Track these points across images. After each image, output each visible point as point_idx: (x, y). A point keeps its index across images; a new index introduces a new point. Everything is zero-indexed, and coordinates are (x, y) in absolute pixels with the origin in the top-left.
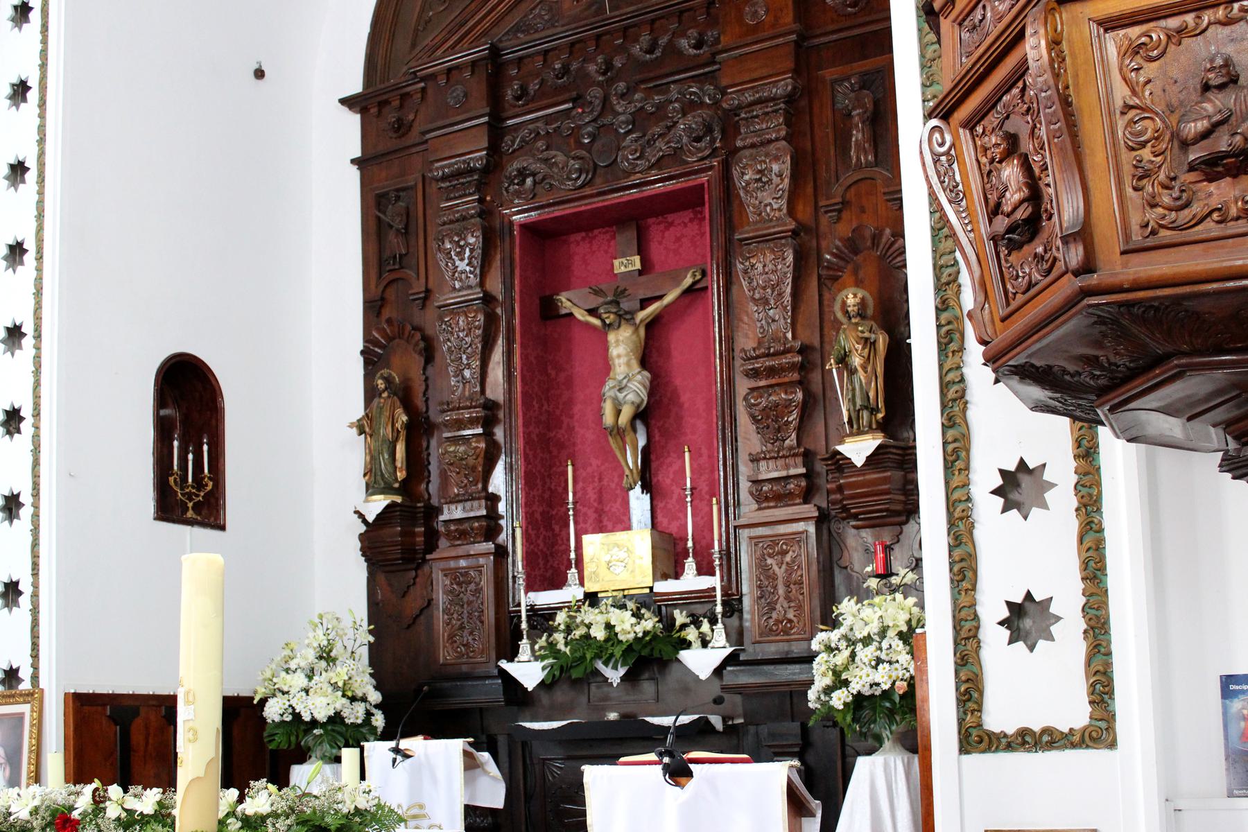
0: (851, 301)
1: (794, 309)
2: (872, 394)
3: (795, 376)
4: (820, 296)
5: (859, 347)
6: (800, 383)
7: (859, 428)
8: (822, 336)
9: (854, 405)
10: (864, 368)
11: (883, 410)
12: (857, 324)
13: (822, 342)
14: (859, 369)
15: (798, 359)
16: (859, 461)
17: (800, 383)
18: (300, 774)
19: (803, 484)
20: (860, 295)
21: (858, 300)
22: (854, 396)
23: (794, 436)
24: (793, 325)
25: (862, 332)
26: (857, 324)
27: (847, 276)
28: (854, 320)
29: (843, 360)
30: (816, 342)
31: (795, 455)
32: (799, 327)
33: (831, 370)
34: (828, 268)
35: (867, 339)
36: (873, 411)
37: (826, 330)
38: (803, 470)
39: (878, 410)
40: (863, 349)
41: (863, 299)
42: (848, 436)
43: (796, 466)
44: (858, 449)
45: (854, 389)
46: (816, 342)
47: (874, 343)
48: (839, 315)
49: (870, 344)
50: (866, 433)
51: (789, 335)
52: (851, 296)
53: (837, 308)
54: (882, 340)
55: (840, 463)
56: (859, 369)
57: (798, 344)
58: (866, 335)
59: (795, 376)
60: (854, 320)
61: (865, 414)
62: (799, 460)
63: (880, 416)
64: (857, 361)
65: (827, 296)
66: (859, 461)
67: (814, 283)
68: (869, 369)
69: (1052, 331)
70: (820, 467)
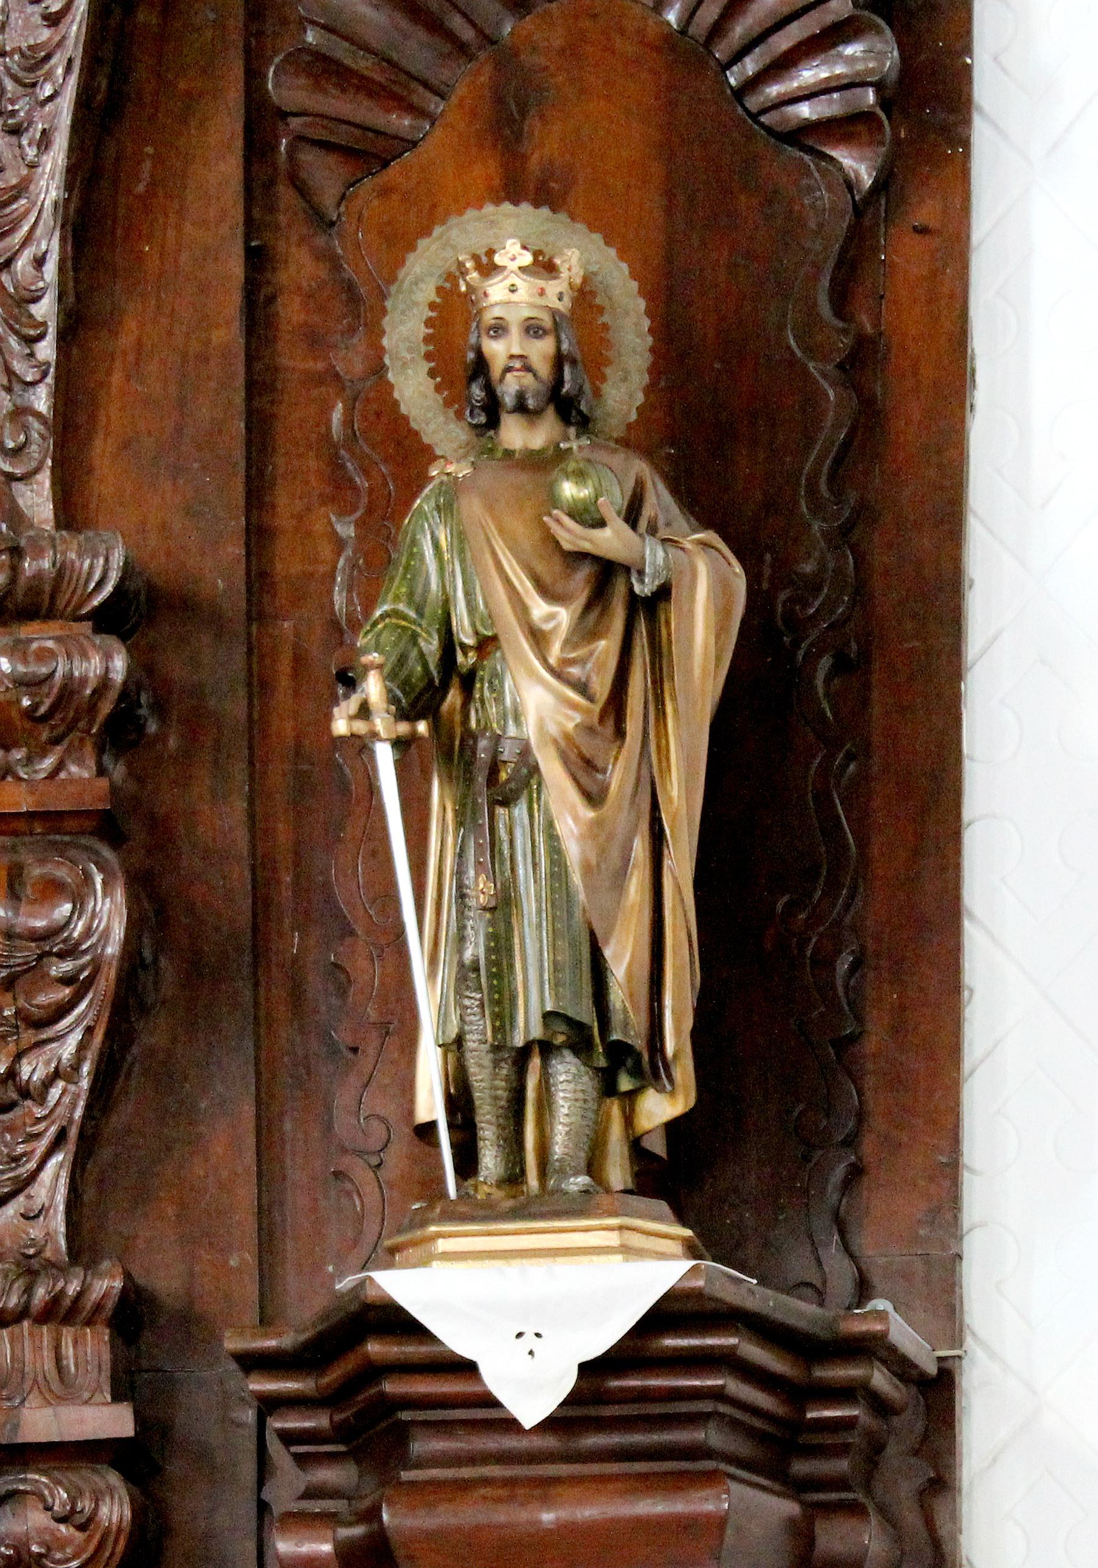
0: (511, 294)
1: (74, 327)
2: (624, 958)
3: (78, 776)
4: (258, 260)
5: (559, 618)
6: (107, 826)
7: (514, 1178)
8: (258, 536)
9: (503, 1020)
10: (586, 772)
11: (684, 1071)
12: (544, 464)
13: (259, 579)
14: (552, 769)
15: (107, 663)
16: (530, 1386)
17: (107, 826)
18: (505, 757)
19: (115, 1512)
20: (572, 261)
21: (556, 293)
22: (501, 947)
23: (52, 1182)
24: (70, 428)
25: (590, 517)
26: (544, 464)
27: (443, 141)
28: (515, 434)
29: (442, 687)
30: (216, 568)
31: (59, 1313)
32: (102, 450)
33: (360, 747)
34: (324, 69)
35: (606, 572)
36: (621, 1066)
37: (285, 504)
38: (115, 1421)
39: (652, 1069)
40: (586, 631)
41: (585, 296)
42: (451, 1215)
43: (63, 1388)
44: (530, 1307)
45: (504, 906)
46: (216, 568)
47: (650, 609)
48: (414, 390)
49: (625, 604)
50: (580, 1207)
51: (37, 500)
52: (513, 255)
53: (405, 328)
54: (708, 596)
55: (380, 1389)
56: (552, 769)
57: (101, 566)
58: (612, 540)
59: (78, 776)
60: (515, 434)
61: (569, 1079)
62: (88, 1350)
63: (658, 1109)
64: (534, 705)
65: (298, 266)
66: (530, 1386)
67: (217, 168)
68: (619, 776)
69: (586, 1230)
70: (222, 1406)
